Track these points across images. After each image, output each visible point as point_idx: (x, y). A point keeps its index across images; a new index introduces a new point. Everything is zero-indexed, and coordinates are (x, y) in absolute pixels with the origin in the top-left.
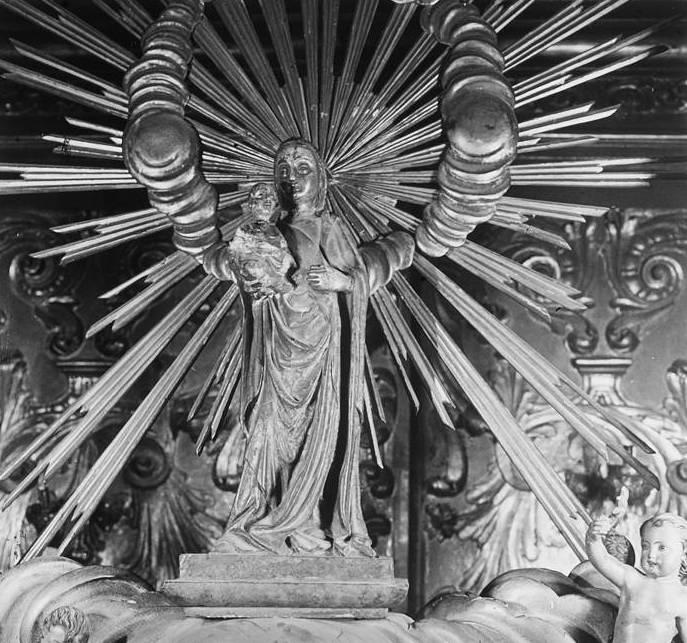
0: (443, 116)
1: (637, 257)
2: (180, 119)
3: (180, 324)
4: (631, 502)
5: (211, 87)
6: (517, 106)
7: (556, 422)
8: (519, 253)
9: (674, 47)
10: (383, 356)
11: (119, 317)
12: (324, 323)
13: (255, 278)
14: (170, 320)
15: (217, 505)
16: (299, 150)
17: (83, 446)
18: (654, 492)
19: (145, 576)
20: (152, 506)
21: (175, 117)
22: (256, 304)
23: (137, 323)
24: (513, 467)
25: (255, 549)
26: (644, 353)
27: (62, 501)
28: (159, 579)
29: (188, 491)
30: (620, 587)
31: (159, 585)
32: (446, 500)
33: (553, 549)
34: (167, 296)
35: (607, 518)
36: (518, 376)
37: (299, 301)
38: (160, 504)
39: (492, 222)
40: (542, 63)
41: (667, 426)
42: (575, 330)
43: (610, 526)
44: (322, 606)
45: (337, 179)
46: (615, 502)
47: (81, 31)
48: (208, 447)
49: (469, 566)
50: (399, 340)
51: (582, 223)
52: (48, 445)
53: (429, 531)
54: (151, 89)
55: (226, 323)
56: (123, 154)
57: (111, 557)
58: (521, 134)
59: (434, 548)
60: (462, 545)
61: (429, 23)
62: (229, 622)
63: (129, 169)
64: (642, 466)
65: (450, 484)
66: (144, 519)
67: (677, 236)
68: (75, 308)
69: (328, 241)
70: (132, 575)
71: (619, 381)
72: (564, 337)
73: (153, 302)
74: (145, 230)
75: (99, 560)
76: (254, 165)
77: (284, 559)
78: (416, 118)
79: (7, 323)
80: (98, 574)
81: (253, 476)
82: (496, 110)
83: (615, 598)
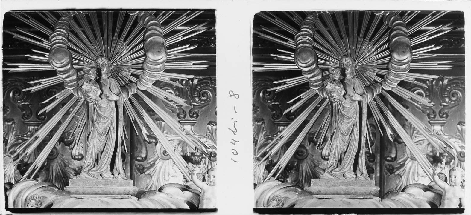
1: (198, 90)
2: (66, 50)
3: (311, 111)
4: (446, 164)
6: (412, 45)
7: (424, 140)
8: (413, 89)
9: (459, 28)
11: (293, 108)
14: (308, 109)
15: (322, 165)
17: (282, 147)
18: (453, 161)
20: (303, 165)
21: (64, 49)
22: (334, 104)
24: (411, 153)
25: (334, 178)
26: (450, 119)
27: (32, 163)
30: (443, 189)
31: (305, 188)
33: (423, 178)
34: (307, 102)
36: (412, 126)
38: (56, 164)
39: (160, 80)
40: (174, 32)
41: (457, 141)
42: (179, 112)
44: (354, 195)
45: (358, 67)
46: (441, 163)
47: (282, 23)
49: (398, 183)
50: (377, 115)
52: (272, 147)
53: (136, 172)
54: (303, 40)
56: (49, 60)
57: (291, 180)
58: (413, 54)
59: (387, 177)
61: (386, 20)
64: (449, 153)
65: (142, 158)
67: (460, 84)
69: (356, 86)
70: (297, 186)
73: (303, 104)
75: (287, 181)
76: (333, 63)
78: (382, 49)
79: (260, 110)
80: (287, 185)
81: (90, 156)
82: (161, 46)
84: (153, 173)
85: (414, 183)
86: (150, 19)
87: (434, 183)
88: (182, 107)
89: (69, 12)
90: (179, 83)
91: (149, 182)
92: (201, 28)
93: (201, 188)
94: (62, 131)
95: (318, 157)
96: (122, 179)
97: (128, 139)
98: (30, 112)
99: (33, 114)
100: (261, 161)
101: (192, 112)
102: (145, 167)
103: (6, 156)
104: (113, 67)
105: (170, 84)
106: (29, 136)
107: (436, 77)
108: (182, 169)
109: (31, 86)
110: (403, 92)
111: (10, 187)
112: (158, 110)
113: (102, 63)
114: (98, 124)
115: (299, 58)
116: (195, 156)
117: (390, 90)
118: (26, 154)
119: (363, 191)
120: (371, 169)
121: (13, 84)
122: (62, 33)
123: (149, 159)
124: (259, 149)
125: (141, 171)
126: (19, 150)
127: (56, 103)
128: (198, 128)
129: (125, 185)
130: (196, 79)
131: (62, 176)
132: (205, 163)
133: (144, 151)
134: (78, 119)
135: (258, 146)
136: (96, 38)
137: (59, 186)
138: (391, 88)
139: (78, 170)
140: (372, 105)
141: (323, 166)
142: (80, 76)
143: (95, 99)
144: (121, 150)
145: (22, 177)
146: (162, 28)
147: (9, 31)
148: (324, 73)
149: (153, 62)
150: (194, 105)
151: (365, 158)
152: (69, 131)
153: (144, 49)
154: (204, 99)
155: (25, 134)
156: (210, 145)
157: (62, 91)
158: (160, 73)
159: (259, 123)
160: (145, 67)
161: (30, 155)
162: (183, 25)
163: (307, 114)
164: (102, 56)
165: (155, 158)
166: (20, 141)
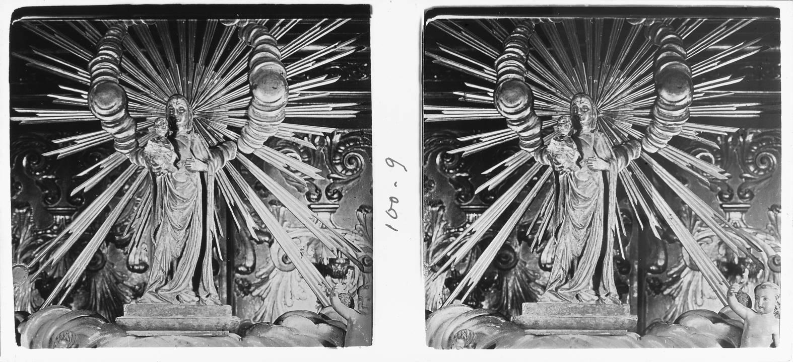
0: (251, 83)
1: (753, 152)
2: (116, 85)
3: (522, 187)
4: (750, 276)
5: (539, 68)
6: (693, 77)
7: (713, 236)
8: (694, 151)
9: (772, 47)
10: (625, 203)
11: (492, 184)
12: (595, 186)
13: (560, 164)
14: (518, 184)
15: (541, 278)
16: (583, 99)
17: (473, 249)
18: (761, 271)
19: (505, 314)
20: (508, 279)
21: (114, 84)
22: (561, 177)
23: (501, 187)
24: (691, 259)
25: (161, 301)
26: (757, 201)
27: (60, 278)
28: (512, 315)
29: (115, 272)
30: (744, 319)
31: (512, 318)
32: (246, 276)
33: (710, 300)
34: (516, 173)
35: (737, 284)
36: (693, 213)
37: (582, 174)
38: (101, 279)
39: (276, 136)
40: (706, 55)
41: (768, 238)
42: (309, 190)
43: (739, 288)
44: (196, 330)
45: (602, 113)
46: (742, 277)
47: (472, 39)
48: (537, 249)
49: (668, 308)
50: (633, 195)
51: (726, 136)
52: (456, 248)
53: (648, 291)
54: (102, 70)
55: (545, 187)
56: (88, 103)
57: (488, 305)
58: (695, 91)
59: (650, 300)
60: (254, 299)
61: (242, 36)
62: (548, 337)
63: (91, 110)
64: (755, 258)
65: (247, 268)
66: (505, 285)
67: (774, 142)
68: (470, 179)
69: (597, 145)
70: (498, 314)
71: (744, 215)
72: (304, 194)
73: (510, 175)
74: (505, 139)
75: (482, 306)
76: (561, 107)
77: (176, 306)
78: (642, 83)
79: (435, 186)
80: (481, 313)
81: (559, 264)
82: (278, 79)
83: (741, 324)
84: (265, 294)
85: (695, 309)
86: (259, 33)
87: (729, 309)
88: (314, 182)
89: (122, 22)
90: (309, 141)
91: (259, 309)
92: (346, 48)
93: (348, 318)
94: (112, 224)
95: (533, 266)
96: (214, 304)
97: (222, 236)
98: (56, 191)
99: (62, 195)
100: (438, 273)
101: (332, 191)
102: (253, 283)
103: (16, 266)
104: (197, 115)
105: (294, 142)
106: (56, 232)
107: (734, 130)
108: (316, 287)
109: (57, 147)
110: (680, 156)
111: (23, 318)
112: (274, 188)
113: (178, 108)
114: (172, 211)
115: (502, 99)
116: (337, 265)
117: (252, 154)
118: (454, 261)
119: (610, 322)
120: (623, 285)
121: (28, 145)
122: (110, 58)
123: (260, 270)
124: (435, 252)
125: (245, 289)
126: (39, 256)
127: (101, 176)
128: (341, 216)
129: (616, 314)
130: (338, 133)
131: (523, 297)
132: (353, 276)
133: (250, 256)
134: (138, 204)
135: (433, 247)
136: (168, 65)
137: (107, 316)
138: (658, 149)
139: (139, 289)
140: (625, 178)
141: (130, 282)
142: (141, 130)
143: (166, 169)
144: (211, 254)
145: (43, 301)
146: (279, 48)
147: (20, 54)
148: (544, 123)
149: (265, 106)
150: (334, 179)
151: (614, 267)
152: (123, 222)
153: (249, 83)
154: (350, 167)
155: (48, 229)
156: (362, 246)
157: (112, 156)
158: (679, 124)
159: (434, 209)
160: (251, 113)
161: (58, 264)
162: (315, 43)
163: (516, 193)
164: (178, 95)
165: (268, 267)
166: (41, 240)
